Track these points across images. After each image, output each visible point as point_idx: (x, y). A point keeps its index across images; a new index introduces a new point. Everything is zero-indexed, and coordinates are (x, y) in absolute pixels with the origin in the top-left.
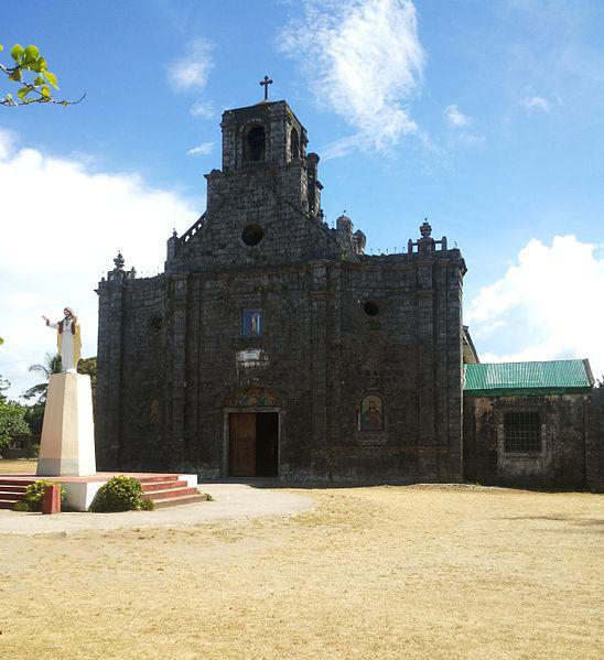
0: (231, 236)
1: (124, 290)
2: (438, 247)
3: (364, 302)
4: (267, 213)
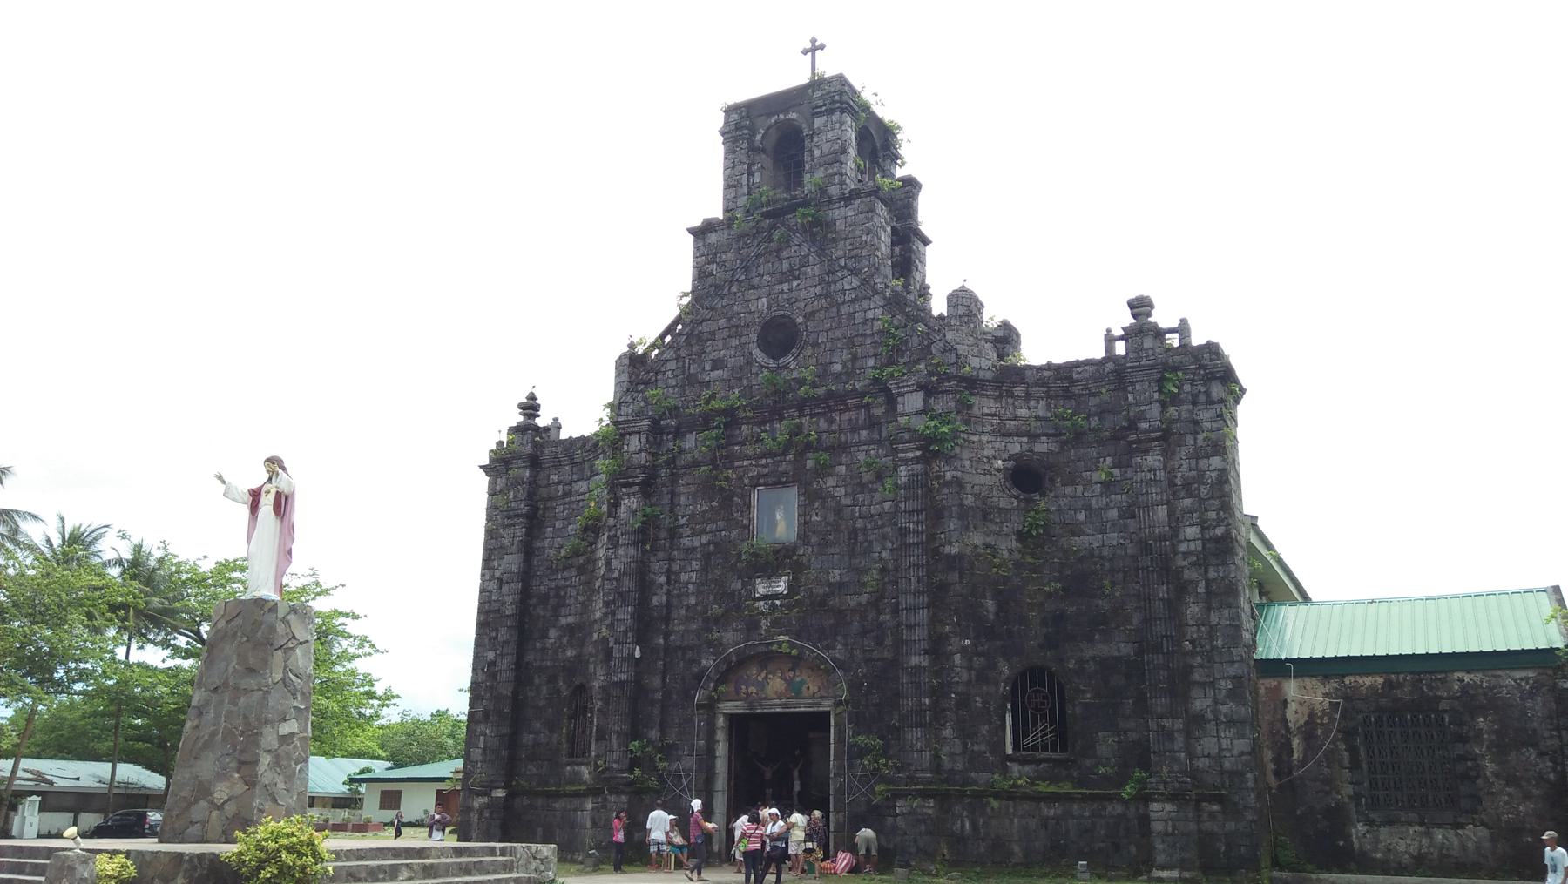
1: (534, 462)
3: (1011, 464)
4: (806, 291)
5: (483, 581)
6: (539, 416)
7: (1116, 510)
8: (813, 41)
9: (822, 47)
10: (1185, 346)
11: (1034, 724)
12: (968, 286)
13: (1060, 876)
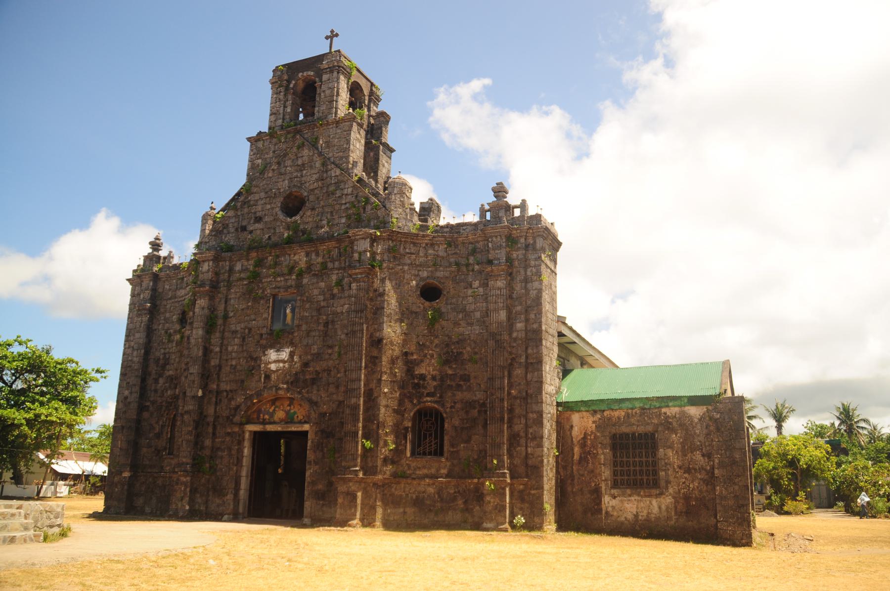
0: (268, 207)
2: (517, 213)
3: (422, 283)
4: (311, 178)
5: (125, 348)
6: (161, 250)
7: (479, 312)
8: (332, 31)
9: (337, 35)
11: (425, 438)
13: (557, 462)
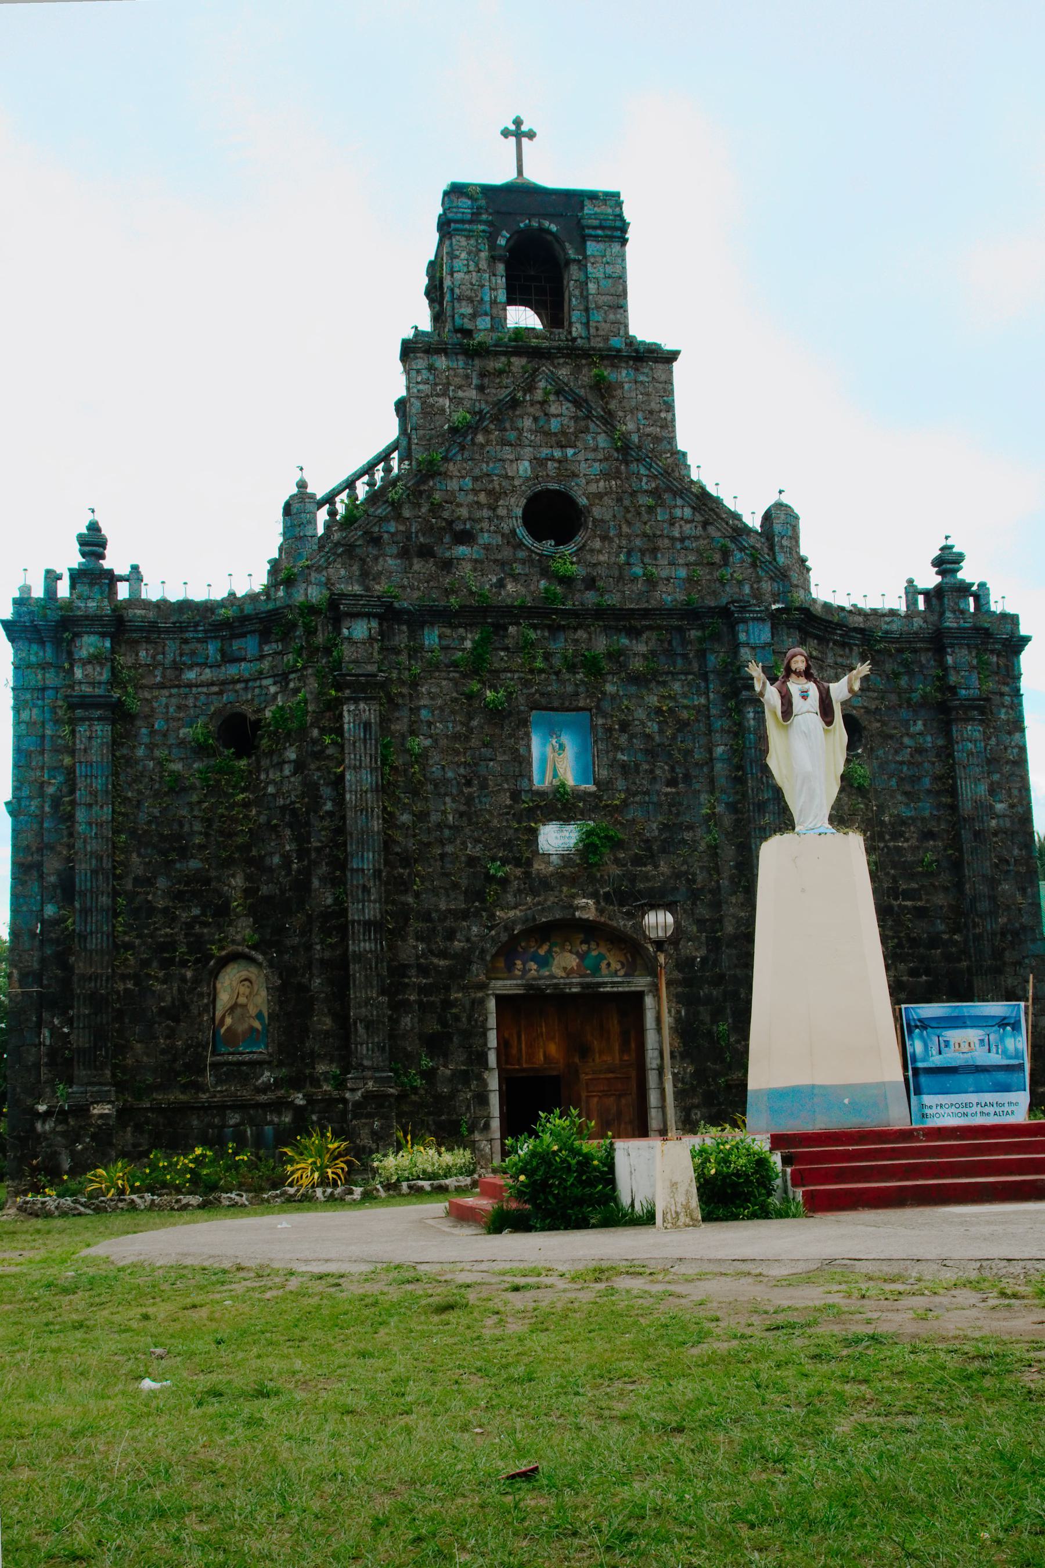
2: (123, 591)
10: (135, 601)
12: (785, 499)
